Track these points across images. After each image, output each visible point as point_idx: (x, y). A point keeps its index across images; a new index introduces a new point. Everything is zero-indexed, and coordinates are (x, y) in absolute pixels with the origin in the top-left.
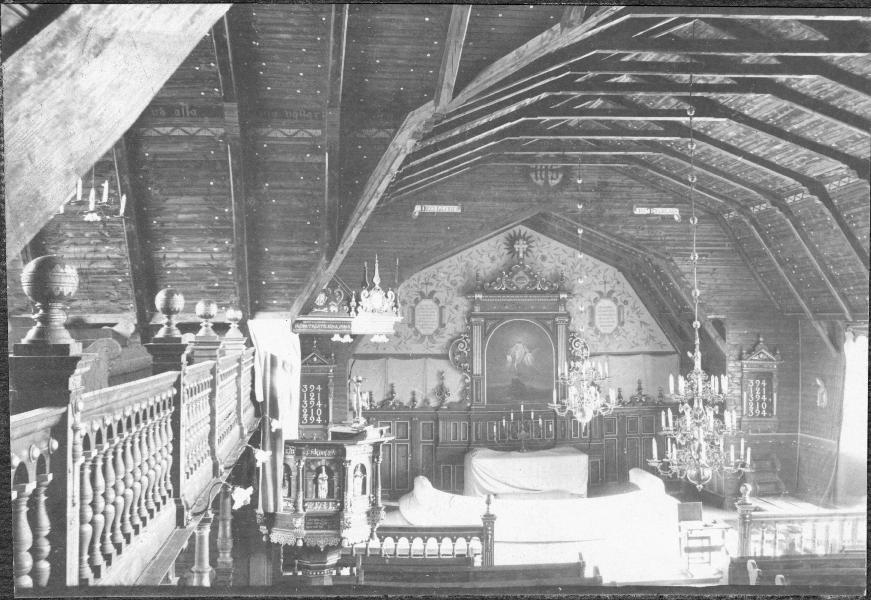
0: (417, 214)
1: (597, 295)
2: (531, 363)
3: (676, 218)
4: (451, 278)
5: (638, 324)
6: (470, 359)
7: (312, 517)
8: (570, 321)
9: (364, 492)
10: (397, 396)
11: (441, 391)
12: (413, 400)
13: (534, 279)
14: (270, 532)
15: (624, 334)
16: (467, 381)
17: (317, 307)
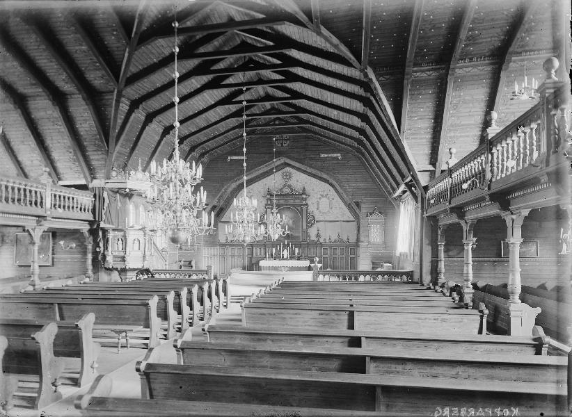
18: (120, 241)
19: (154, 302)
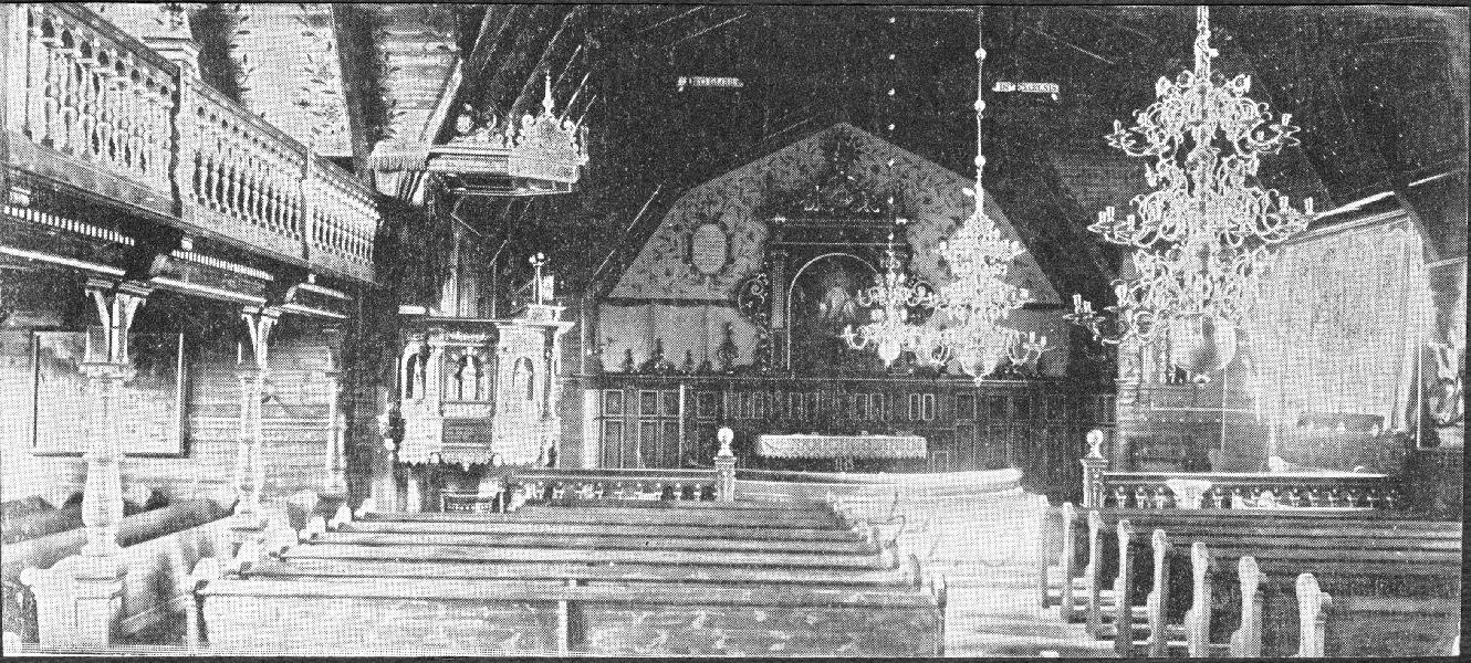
3: (1054, 97)
6: (768, 307)
8: (910, 258)
9: (530, 397)
10: (665, 356)
11: (728, 347)
12: (689, 361)
14: (398, 448)
16: (763, 336)
17: (459, 134)
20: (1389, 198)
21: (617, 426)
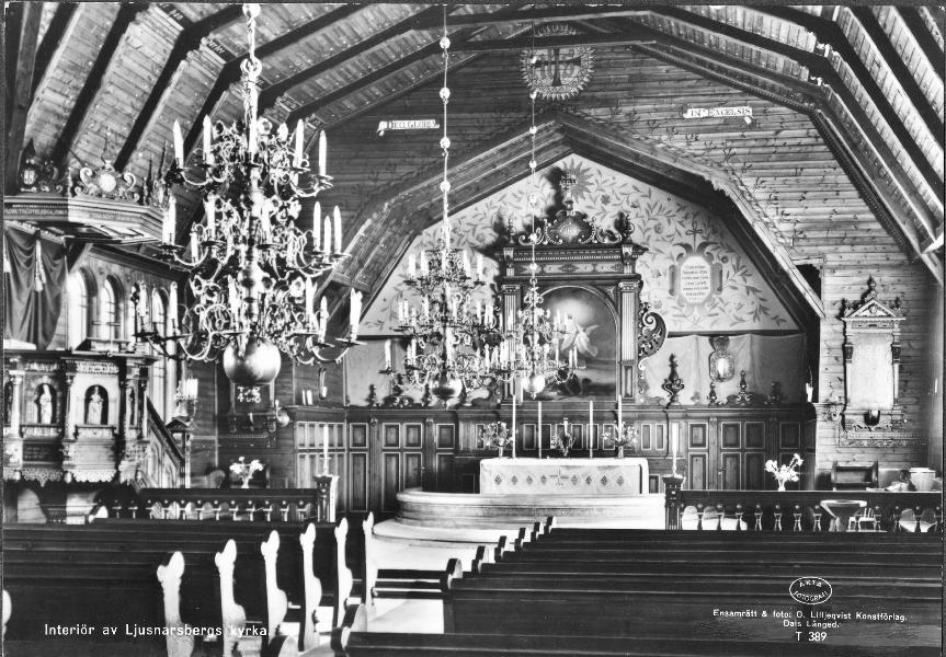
0: (382, 134)
1: (683, 250)
2: (586, 347)
4: (478, 231)
5: (742, 290)
7: (32, 446)
13: (587, 229)
15: (721, 305)
18: (47, 395)
19: (171, 574)
20: (935, 280)
21: (701, 459)
